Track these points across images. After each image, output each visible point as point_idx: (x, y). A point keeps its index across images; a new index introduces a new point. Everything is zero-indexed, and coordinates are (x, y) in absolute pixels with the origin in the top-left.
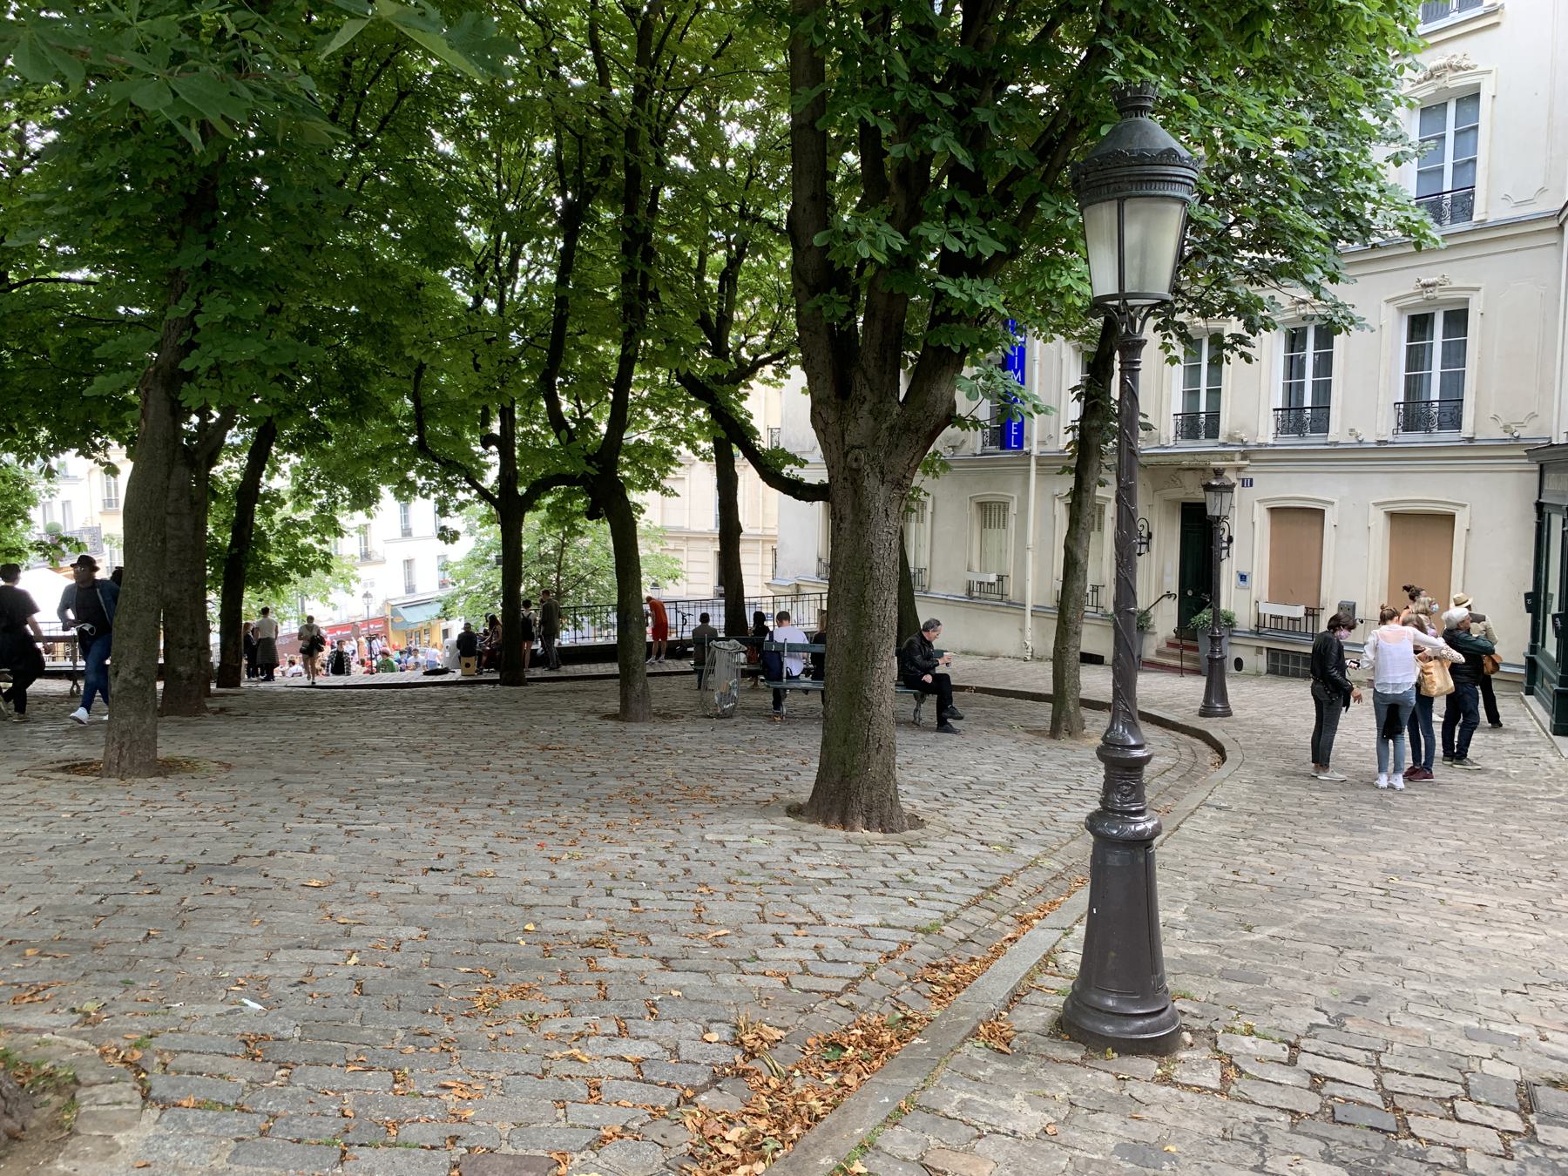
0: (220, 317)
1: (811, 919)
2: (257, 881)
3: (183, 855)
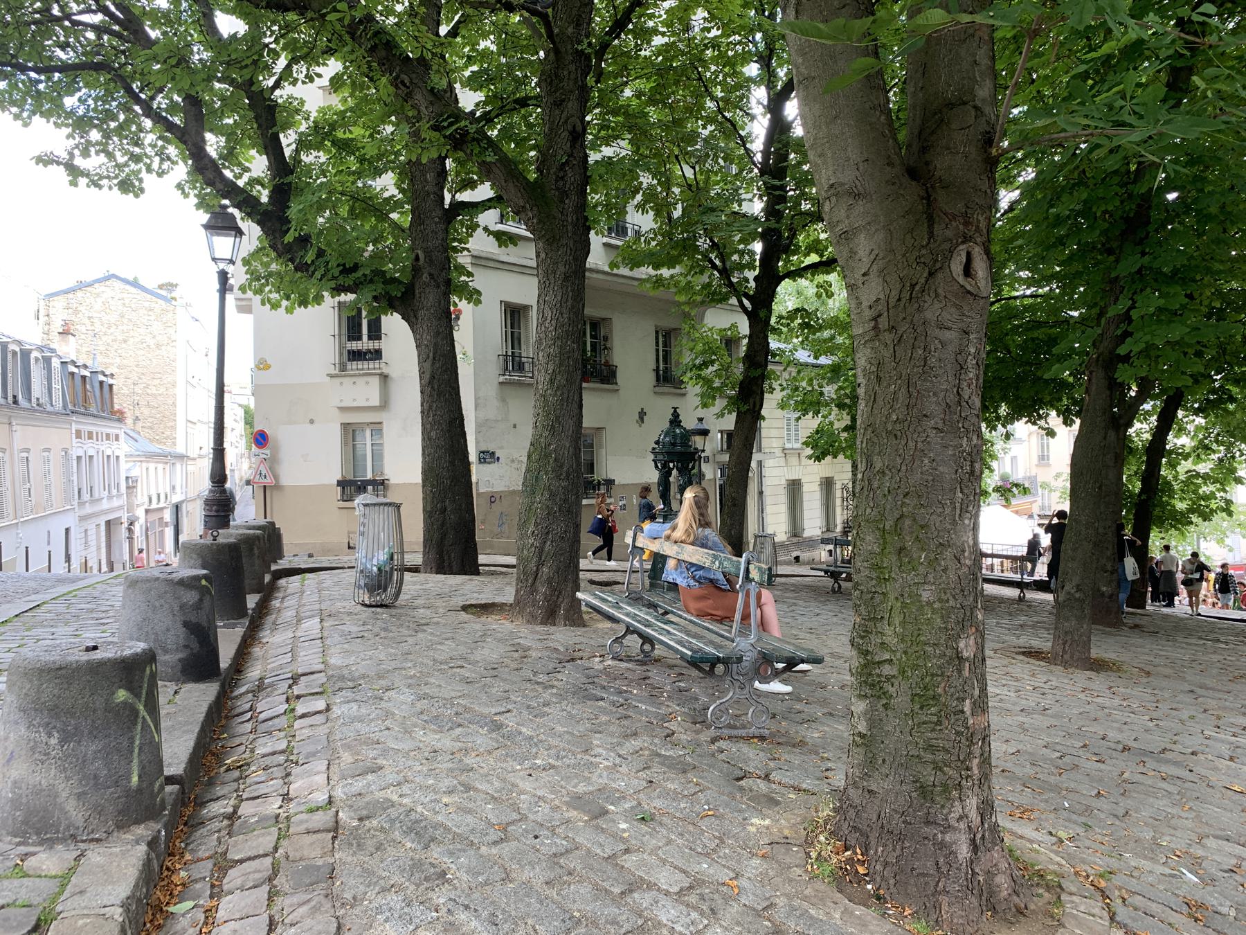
0: (1152, 310)
2: (1184, 773)
3: (1119, 737)
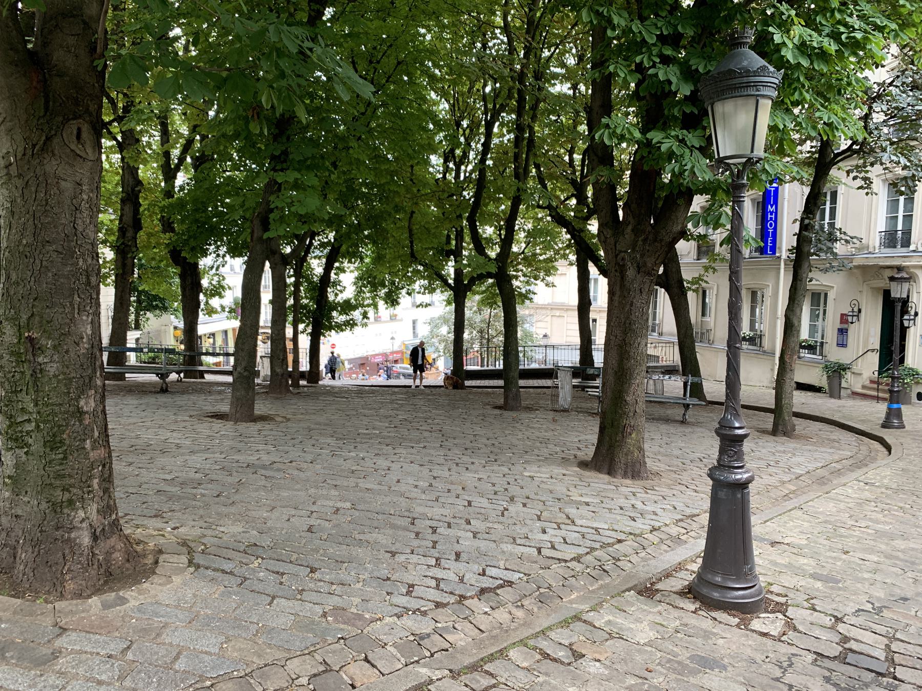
1: (569, 522)
